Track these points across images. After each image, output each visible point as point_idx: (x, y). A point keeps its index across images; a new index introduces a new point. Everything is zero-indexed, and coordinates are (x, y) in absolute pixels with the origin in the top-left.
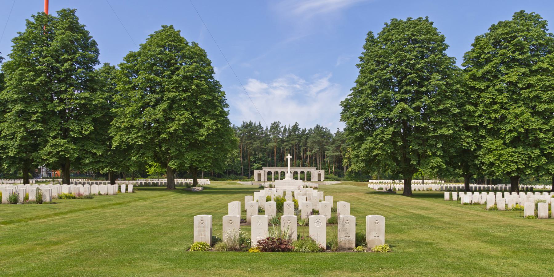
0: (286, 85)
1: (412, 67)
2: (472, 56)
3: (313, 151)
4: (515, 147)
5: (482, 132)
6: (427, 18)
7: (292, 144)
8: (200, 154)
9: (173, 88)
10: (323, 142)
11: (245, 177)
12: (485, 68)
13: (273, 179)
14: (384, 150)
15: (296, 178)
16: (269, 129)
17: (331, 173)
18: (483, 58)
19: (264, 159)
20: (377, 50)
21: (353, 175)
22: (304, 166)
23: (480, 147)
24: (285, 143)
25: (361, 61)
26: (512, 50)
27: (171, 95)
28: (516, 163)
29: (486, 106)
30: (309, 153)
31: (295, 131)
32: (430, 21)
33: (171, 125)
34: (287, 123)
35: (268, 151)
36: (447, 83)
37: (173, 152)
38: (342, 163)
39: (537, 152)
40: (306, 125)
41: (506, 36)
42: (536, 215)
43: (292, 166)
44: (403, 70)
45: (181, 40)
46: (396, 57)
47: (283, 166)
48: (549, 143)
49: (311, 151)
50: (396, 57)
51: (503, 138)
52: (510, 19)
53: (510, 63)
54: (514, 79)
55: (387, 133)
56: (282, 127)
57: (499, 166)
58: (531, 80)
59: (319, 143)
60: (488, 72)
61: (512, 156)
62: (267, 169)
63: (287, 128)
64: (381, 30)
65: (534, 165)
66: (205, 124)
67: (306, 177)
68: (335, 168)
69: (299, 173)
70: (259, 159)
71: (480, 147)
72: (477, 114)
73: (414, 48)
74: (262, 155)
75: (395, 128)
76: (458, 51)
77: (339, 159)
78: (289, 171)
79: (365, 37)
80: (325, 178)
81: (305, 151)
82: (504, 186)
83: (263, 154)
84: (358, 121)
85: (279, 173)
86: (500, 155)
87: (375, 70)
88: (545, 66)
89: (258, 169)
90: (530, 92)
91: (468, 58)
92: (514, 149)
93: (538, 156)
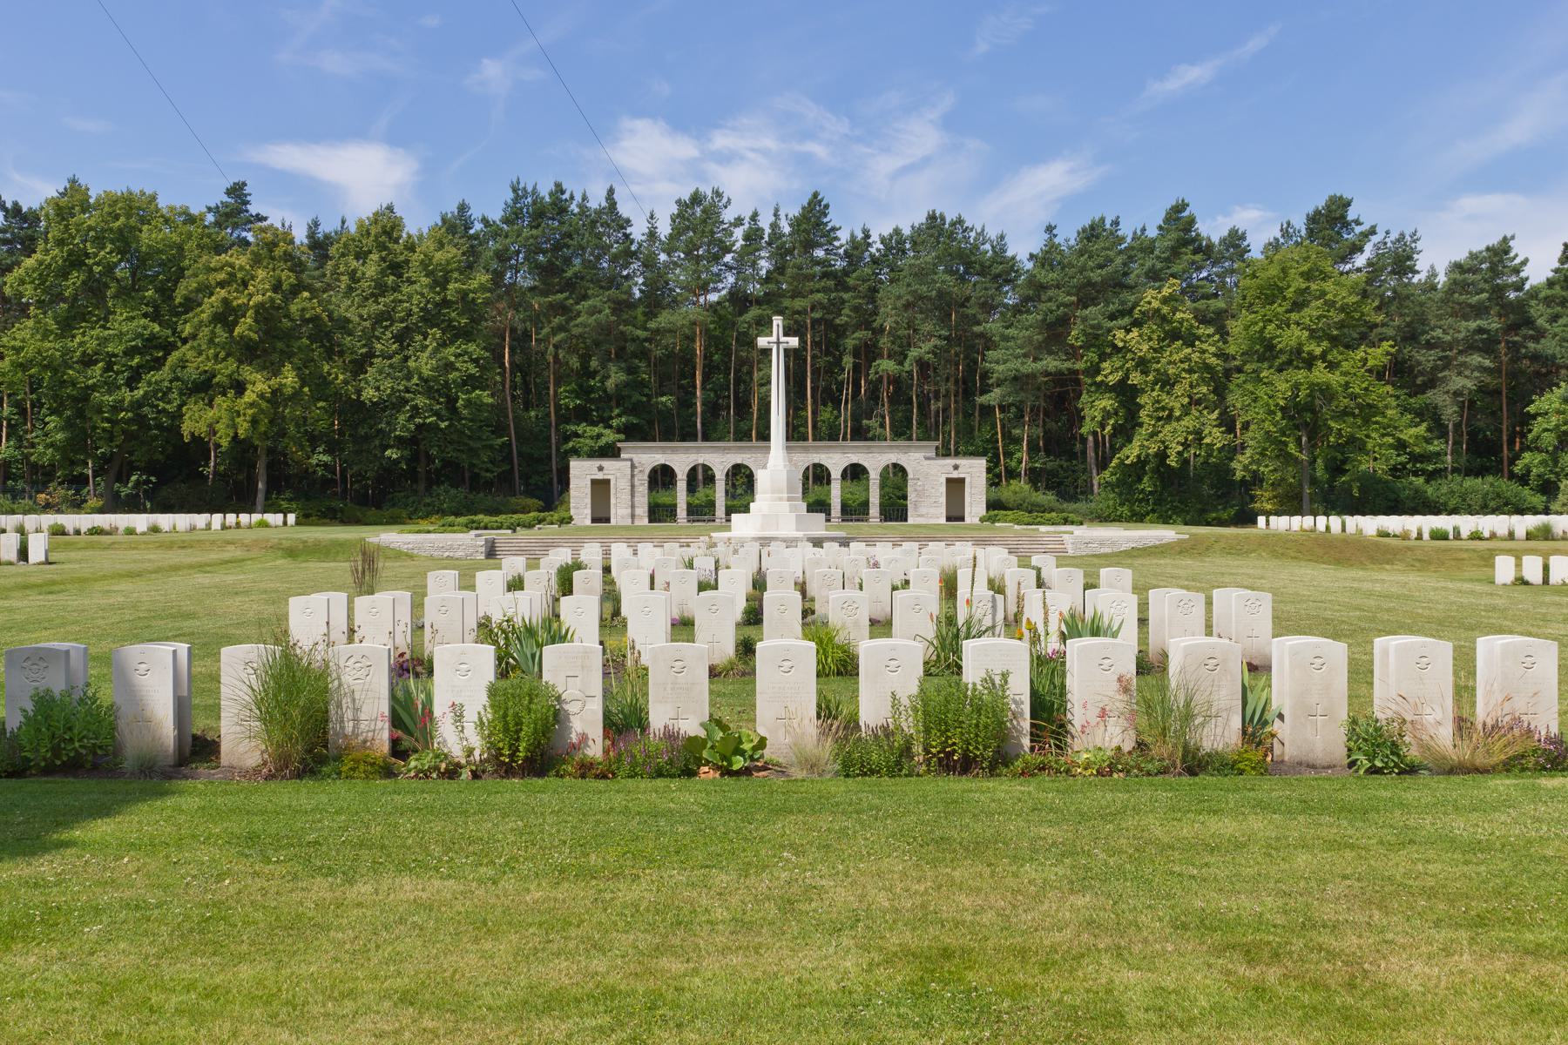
3: (914, 353)
13: (682, 512)
16: (664, 229)
17: (1012, 474)
19: (636, 397)
24: (754, 312)
30: (886, 365)
31: (809, 245)
42: (1546, 581)
43: (795, 433)
47: (742, 436)
49: (900, 357)
59: (944, 305)
62: (649, 457)
63: (765, 223)
68: (1033, 448)
69: (836, 474)
70: (607, 398)
74: (623, 377)
77: (1060, 397)
80: (994, 505)
81: (868, 353)
83: (631, 371)
85: (720, 476)
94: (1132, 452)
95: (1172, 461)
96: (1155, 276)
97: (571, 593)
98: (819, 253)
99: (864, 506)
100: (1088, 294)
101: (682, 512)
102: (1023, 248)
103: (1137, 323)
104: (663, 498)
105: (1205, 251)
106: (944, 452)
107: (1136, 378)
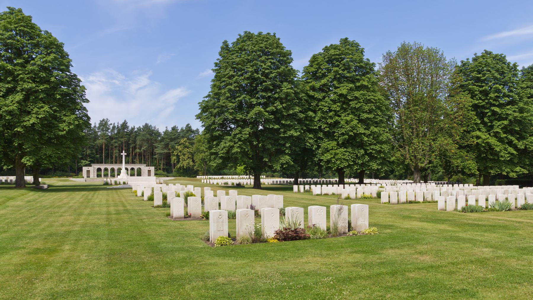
0: (104, 80)
1: (266, 75)
2: (311, 70)
3: (143, 148)
4: (346, 148)
5: (321, 135)
6: (275, 34)
7: (120, 141)
8: (58, 150)
9: (28, 78)
10: (151, 139)
11: (72, 174)
12: (324, 81)
13: (103, 176)
14: (242, 148)
15: (132, 175)
16: (97, 125)
17: (160, 169)
18: (320, 73)
19: (93, 156)
20: (234, 58)
21: (181, 171)
22: (133, 162)
23: (319, 147)
24: (114, 141)
25: (216, 66)
26: (342, 68)
27: (26, 86)
28: (347, 160)
29: (323, 112)
30: (138, 150)
31: (124, 129)
32: (277, 37)
33: (27, 119)
34: (115, 120)
35: (97, 147)
36: (295, 91)
37: (27, 147)
38: (170, 160)
39: (362, 151)
40: (135, 123)
41: (337, 57)
42: (389, 202)
43: (127, 162)
44: (259, 77)
45: (33, 27)
46: (252, 66)
48: (370, 145)
49: (140, 149)
50: (252, 66)
51: (336, 140)
52: (338, 43)
53: (340, 79)
54: (344, 92)
55: (245, 132)
56: (111, 124)
57: (335, 163)
58: (357, 94)
59: (148, 140)
60: (324, 85)
61: (344, 155)
63: (116, 125)
64: (235, 40)
65: (360, 162)
66: (65, 118)
68: (164, 164)
71: (319, 147)
72: (316, 119)
73: (268, 59)
75: (251, 129)
76: (299, 64)
77: (168, 157)
79: (221, 45)
81: (135, 148)
82: (309, 180)
83: (92, 151)
84: (216, 121)
86: (336, 154)
87: (233, 76)
88: (365, 83)
89: (86, 165)
90: (356, 104)
91: (306, 71)
92: (345, 149)
93: (363, 155)
94: (179, 166)
95: (185, 167)
96: (183, 137)
97: (140, 175)
98: (126, 130)
99: (108, 175)
100: (172, 140)
101: (103, 176)
102: (162, 130)
103: (180, 145)
104: (99, 173)
105: (193, 132)
106: (148, 166)
107: (179, 154)
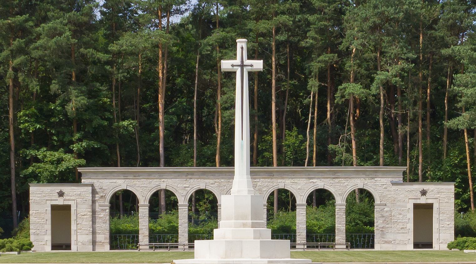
3: (380, 76)
13: (144, 238)
15: (284, 232)
19: (97, 121)
22: (325, 158)
30: (353, 89)
43: (259, 158)
47: (206, 160)
49: (367, 80)
62: (110, 182)
67: (341, 225)
69: (301, 200)
70: (68, 122)
74: (83, 100)
78: (240, 191)
81: (334, 76)
83: (92, 94)
101: (144, 238)
104: (125, 224)
106: (412, 177)
